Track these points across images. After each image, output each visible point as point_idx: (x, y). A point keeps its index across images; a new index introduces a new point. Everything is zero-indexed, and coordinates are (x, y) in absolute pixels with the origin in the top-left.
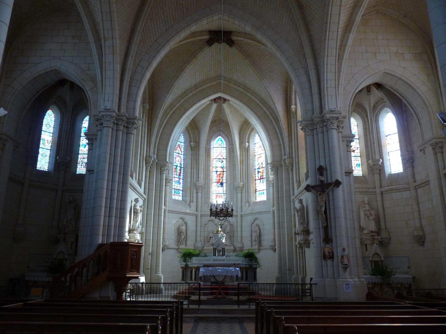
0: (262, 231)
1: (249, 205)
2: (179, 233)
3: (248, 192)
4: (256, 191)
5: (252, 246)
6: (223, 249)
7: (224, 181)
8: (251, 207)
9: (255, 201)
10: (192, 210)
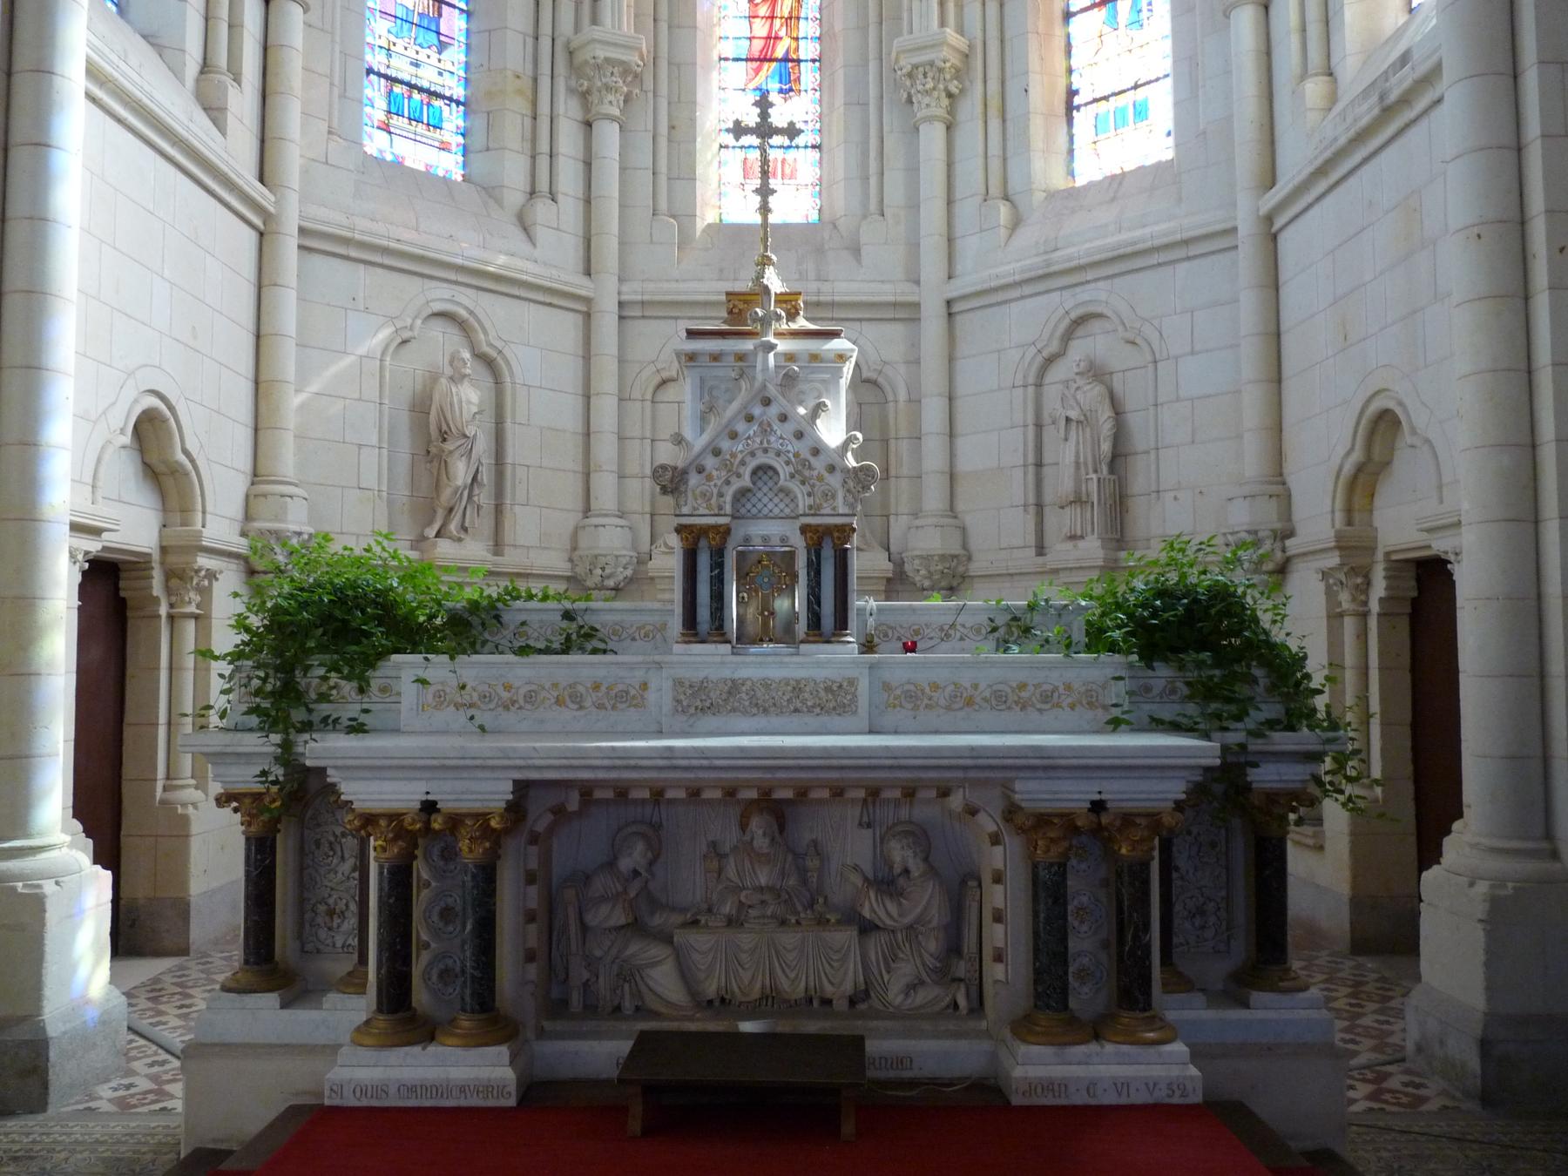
0: (1136, 421)
1: (1016, 223)
2: (430, 435)
3: (1005, 113)
4: (1070, 108)
5: (1041, 550)
6: (828, 544)
7: (808, 50)
8: (1027, 236)
9: (1059, 182)
10: (551, 256)
